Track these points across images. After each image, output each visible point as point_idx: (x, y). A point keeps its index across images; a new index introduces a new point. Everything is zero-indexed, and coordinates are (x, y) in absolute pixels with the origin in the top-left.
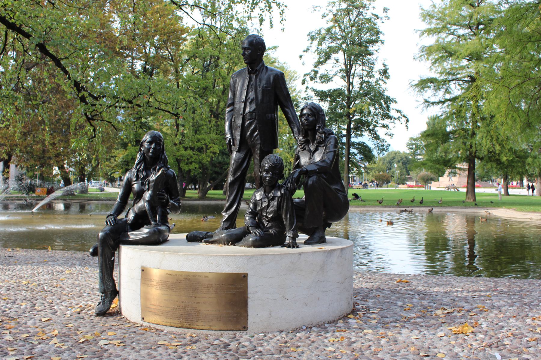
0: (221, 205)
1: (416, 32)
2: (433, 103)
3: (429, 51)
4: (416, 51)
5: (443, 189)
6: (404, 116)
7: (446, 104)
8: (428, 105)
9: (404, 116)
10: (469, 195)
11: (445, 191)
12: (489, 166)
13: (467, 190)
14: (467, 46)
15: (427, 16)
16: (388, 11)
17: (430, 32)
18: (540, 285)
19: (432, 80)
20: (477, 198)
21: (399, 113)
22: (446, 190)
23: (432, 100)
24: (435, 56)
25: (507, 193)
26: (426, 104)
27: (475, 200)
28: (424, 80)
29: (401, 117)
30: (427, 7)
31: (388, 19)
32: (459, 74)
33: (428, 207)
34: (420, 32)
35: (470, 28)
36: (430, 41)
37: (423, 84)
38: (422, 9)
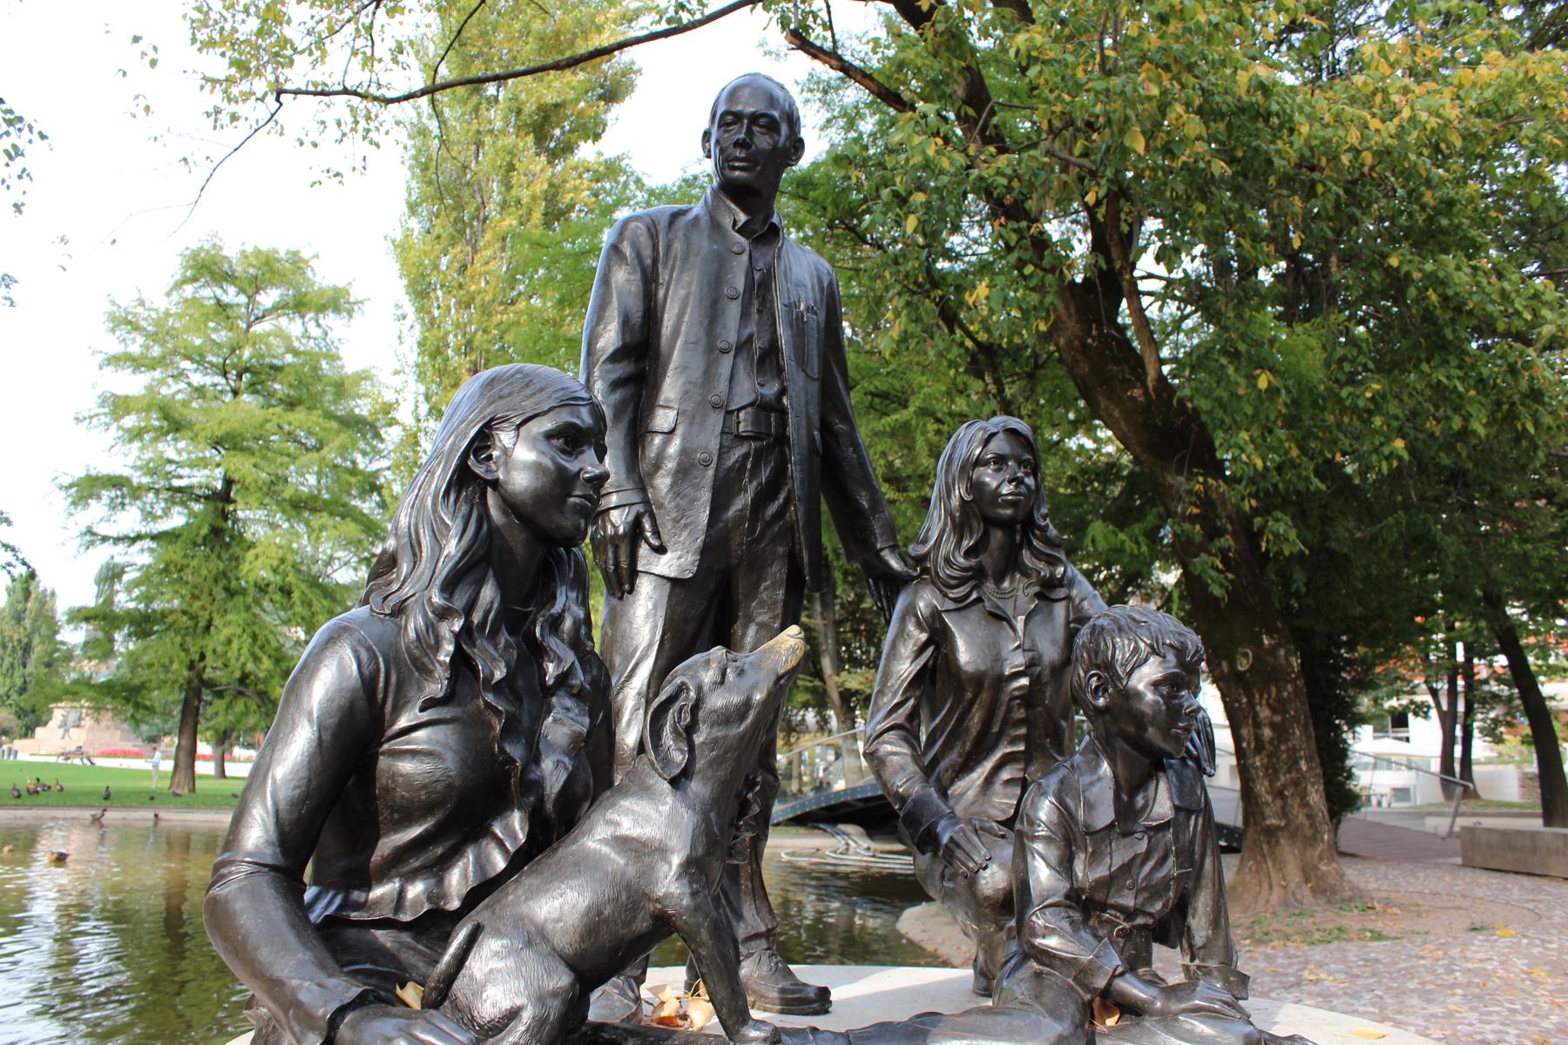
0: (613, 847)
1: (94, 353)
2: (105, 539)
3: (118, 406)
4: (90, 404)
5: (53, 759)
6: (24, 563)
7: (139, 545)
8: (92, 543)
9: (24, 563)
10: (181, 777)
11: (57, 764)
12: (239, 706)
13: (176, 766)
14: (224, 414)
15: (124, 322)
16: (13, 286)
17: (116, 361)
18: (1561, 991)
19: (116, 482)
20: (198, 783)
21: (10, 553)
22: (61, 760)
23: (102, 530)
24: (130, 421)
25: (222, 773)
26: (88, 538)
27: (193, 789)
28: (97, 479)
29: (14, 562)
30: (126, 301)
31: (12, 304)
32: (181, 477)
33: (89, 806)
34: (103, 356)
35: (225, 374)
36: (133, 384)
37: (88, 488)
38: (113, 303)
